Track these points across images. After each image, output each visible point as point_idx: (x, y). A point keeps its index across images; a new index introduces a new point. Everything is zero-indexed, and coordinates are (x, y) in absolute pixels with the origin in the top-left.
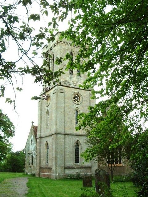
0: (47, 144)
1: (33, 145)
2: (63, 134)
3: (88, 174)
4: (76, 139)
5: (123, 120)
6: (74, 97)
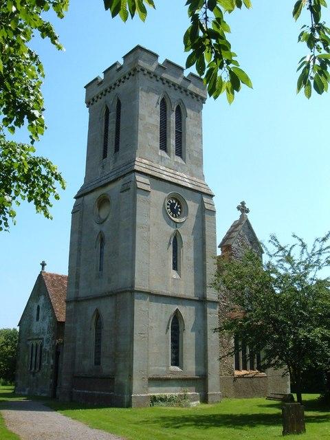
0: (98, 315)
1: (44, 318)
2: (82, 301)
3: (191, 391)
4: (173, 308)
5: (64, 288)
6: (168, 205)
